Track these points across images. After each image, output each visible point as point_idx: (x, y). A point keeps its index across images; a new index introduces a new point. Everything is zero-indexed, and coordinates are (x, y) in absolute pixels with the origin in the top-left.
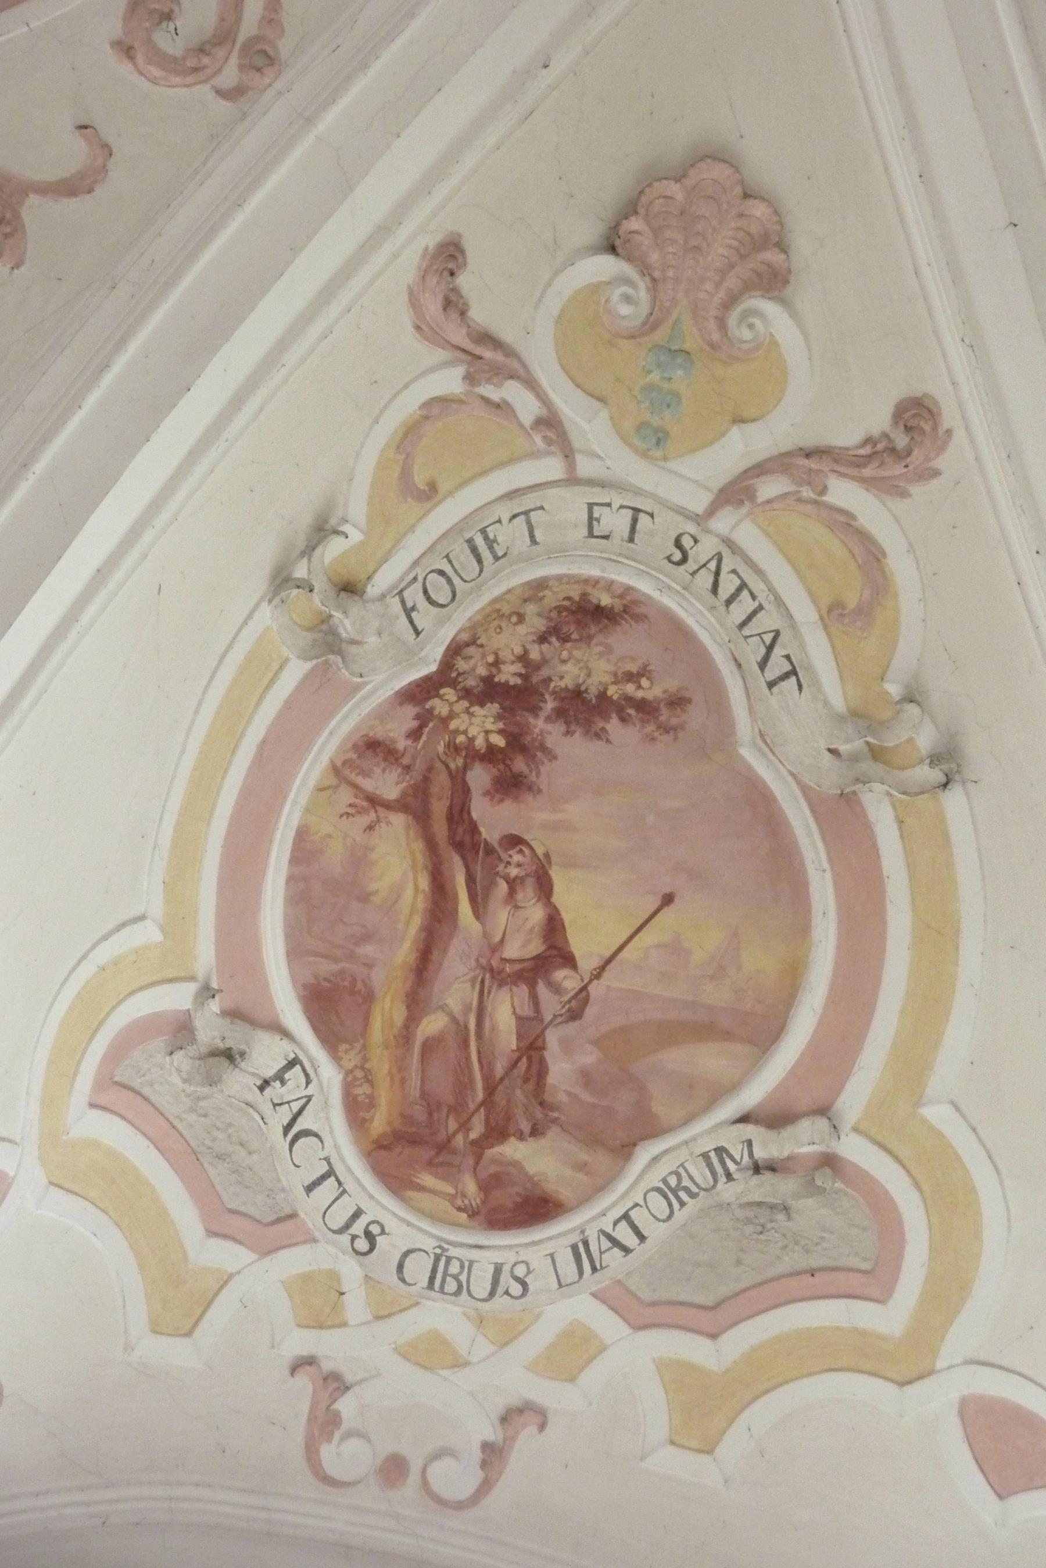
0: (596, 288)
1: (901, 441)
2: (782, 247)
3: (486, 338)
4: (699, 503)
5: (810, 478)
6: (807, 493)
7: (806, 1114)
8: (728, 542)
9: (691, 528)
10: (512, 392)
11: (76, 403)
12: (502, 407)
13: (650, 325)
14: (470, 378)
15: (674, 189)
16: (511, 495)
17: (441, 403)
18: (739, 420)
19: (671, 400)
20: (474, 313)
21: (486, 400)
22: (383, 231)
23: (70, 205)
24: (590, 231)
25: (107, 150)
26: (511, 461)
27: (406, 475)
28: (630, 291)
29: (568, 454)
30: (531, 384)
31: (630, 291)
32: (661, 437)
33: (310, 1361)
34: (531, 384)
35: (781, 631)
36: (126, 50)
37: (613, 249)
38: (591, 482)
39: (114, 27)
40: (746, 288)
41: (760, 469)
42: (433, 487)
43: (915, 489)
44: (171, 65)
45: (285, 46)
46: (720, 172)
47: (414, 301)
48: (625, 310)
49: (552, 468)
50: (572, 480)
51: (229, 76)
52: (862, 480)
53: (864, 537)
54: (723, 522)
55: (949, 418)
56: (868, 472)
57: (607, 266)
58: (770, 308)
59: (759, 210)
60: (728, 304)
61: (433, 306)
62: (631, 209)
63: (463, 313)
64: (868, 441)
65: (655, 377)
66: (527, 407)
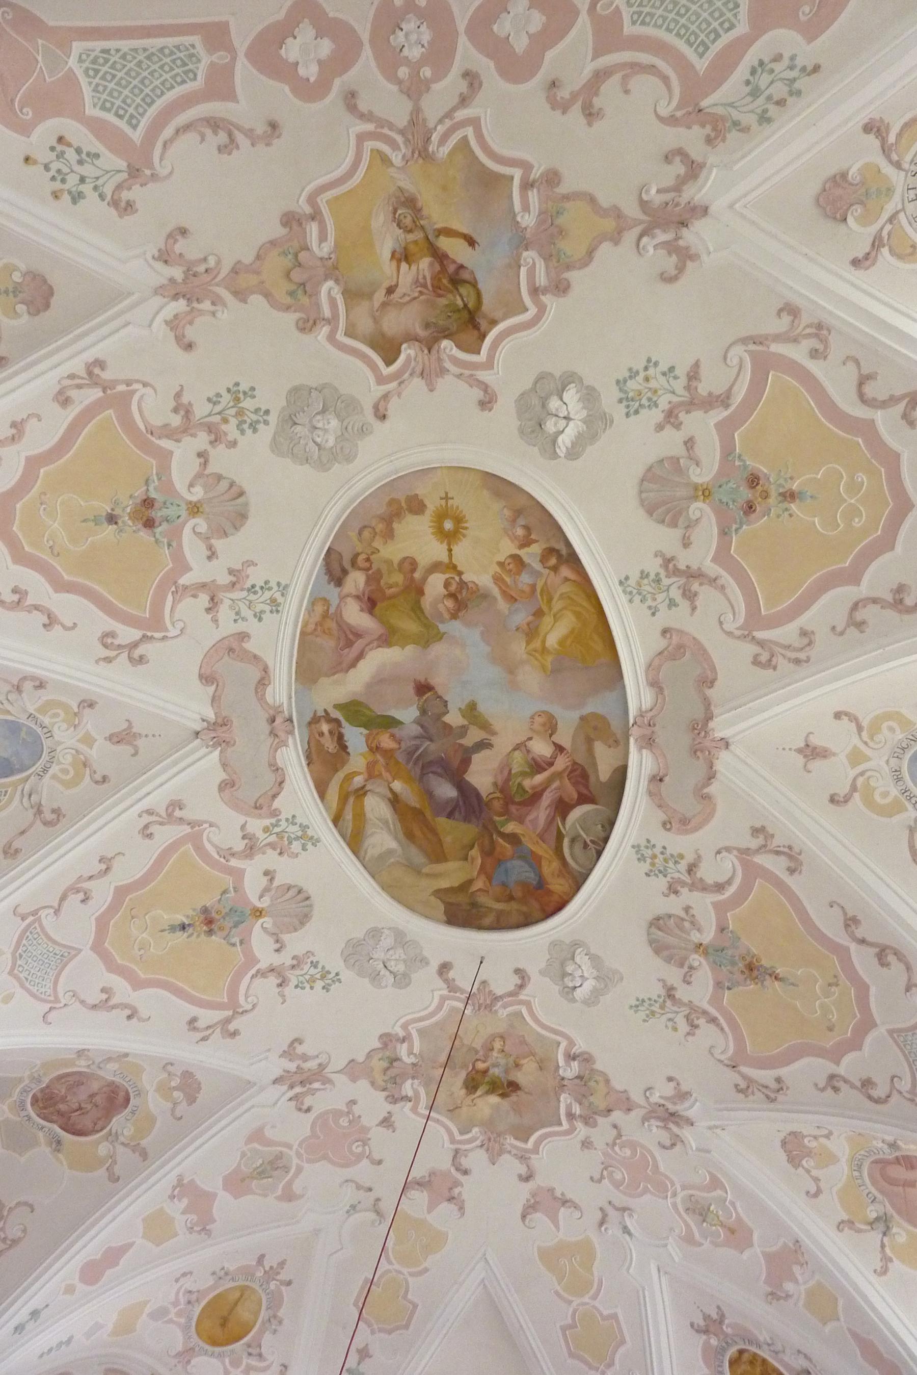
0: (856, 219)
1: (875, 129)
2: (835, 176)
3: (873, 245)
4: (903, 174)
5: (890, 149)
6: (894, 148)
8: (911, 163)
9: (909, 174)
10: (885, 233)
12: (889, 234)
13: (862, 203)
14: (884, 246)
15: (828, 209)
16: (910, 224)
17: (890, 251)
18: (879, 171)
19: (879, 191)
20: (867, 250)
21: (888, 239)
24: (842, 227)
25: (848, 357)
26: (901, 227)
28: (385, 148)
29: (897, 212)
30: (882, 229)
31: (385, 148)
32: (889, 189)
34: (882, 229)
35: (378, 1035)
36: (825, 358)
37: (845, 219)
38: (903, 204)
39: (821, 361)
40: (847, 181)
41: (891, 162)
42: (912, 246)
43: (886, 122)
45: (816, 321)
47: (867, 269)
48: (859, 211)
50: (903, 209)
51: (825, 332)
52: (887, 135)
53: (902, 130)
54: (906, 166)
55: (866, 120)
56: (884, 135)
57: (850, 220)
58: (850, 174)
59: (827, 186)
60: (853, 185)
61: (868, 263)
62: (835, 218)
64: (877, 137)
65: (874, 196)
66: (888, 227)
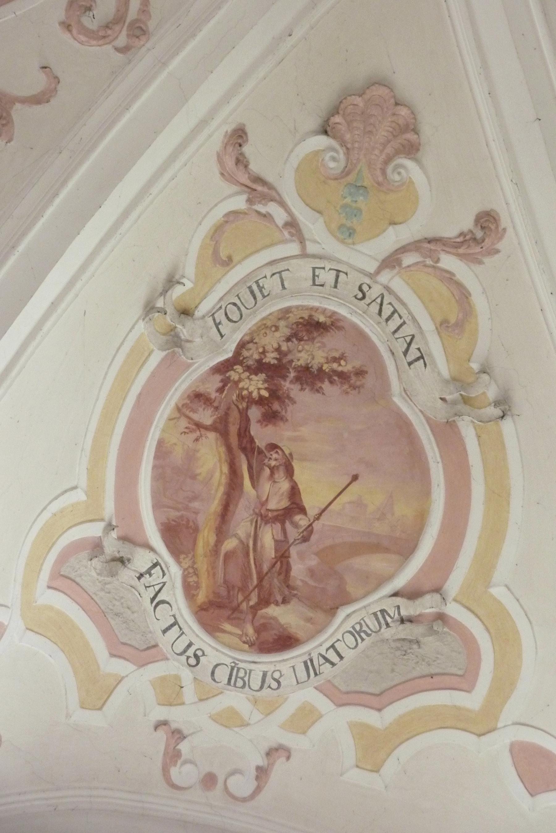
0: (317, 153)
1: (479, 234)
2: (416, 131)
3: (258, 180)
4: (372, 267)
5: (430, 254)
9: (367, 280)
10: (272, 208)
11: (40, 214)
12: (267, 216)
13: (346, 173)
14: (250, 201)
15: (358, 101)
16: (272, 263)
18: (393, 223)
19: (357, 212)
21: (258, 213)
24: (314, 123)
25: (57, 80)
26: (272, 245)
29: (302, 241)
30: (282, 204)
32: (351, 232)
34: (282, 204)
36: (67, 26)
37: (326, 132)
38: (314, 256)
39: (60, 14)
40: (397, 153)
41: (404, 249)
42: (230, 259)
43: (486, 260)
45: (151, 25)
46: (383, 91)
47: (220, 160)
48: (332, 165)
49: (293, 249)
50: (304, 255)
51: (122, 40)
52: (458, 255)
53: (459, 285)
54: (385, 277)
55: (505, 222)
56: (461, 251)
57: (322, 141)
58: (409, 164)
59: (403, 112)
60: (387, 162)
61: (230, 163)
64: (461, 234)
65: (348, 200)
66: (280, 216)
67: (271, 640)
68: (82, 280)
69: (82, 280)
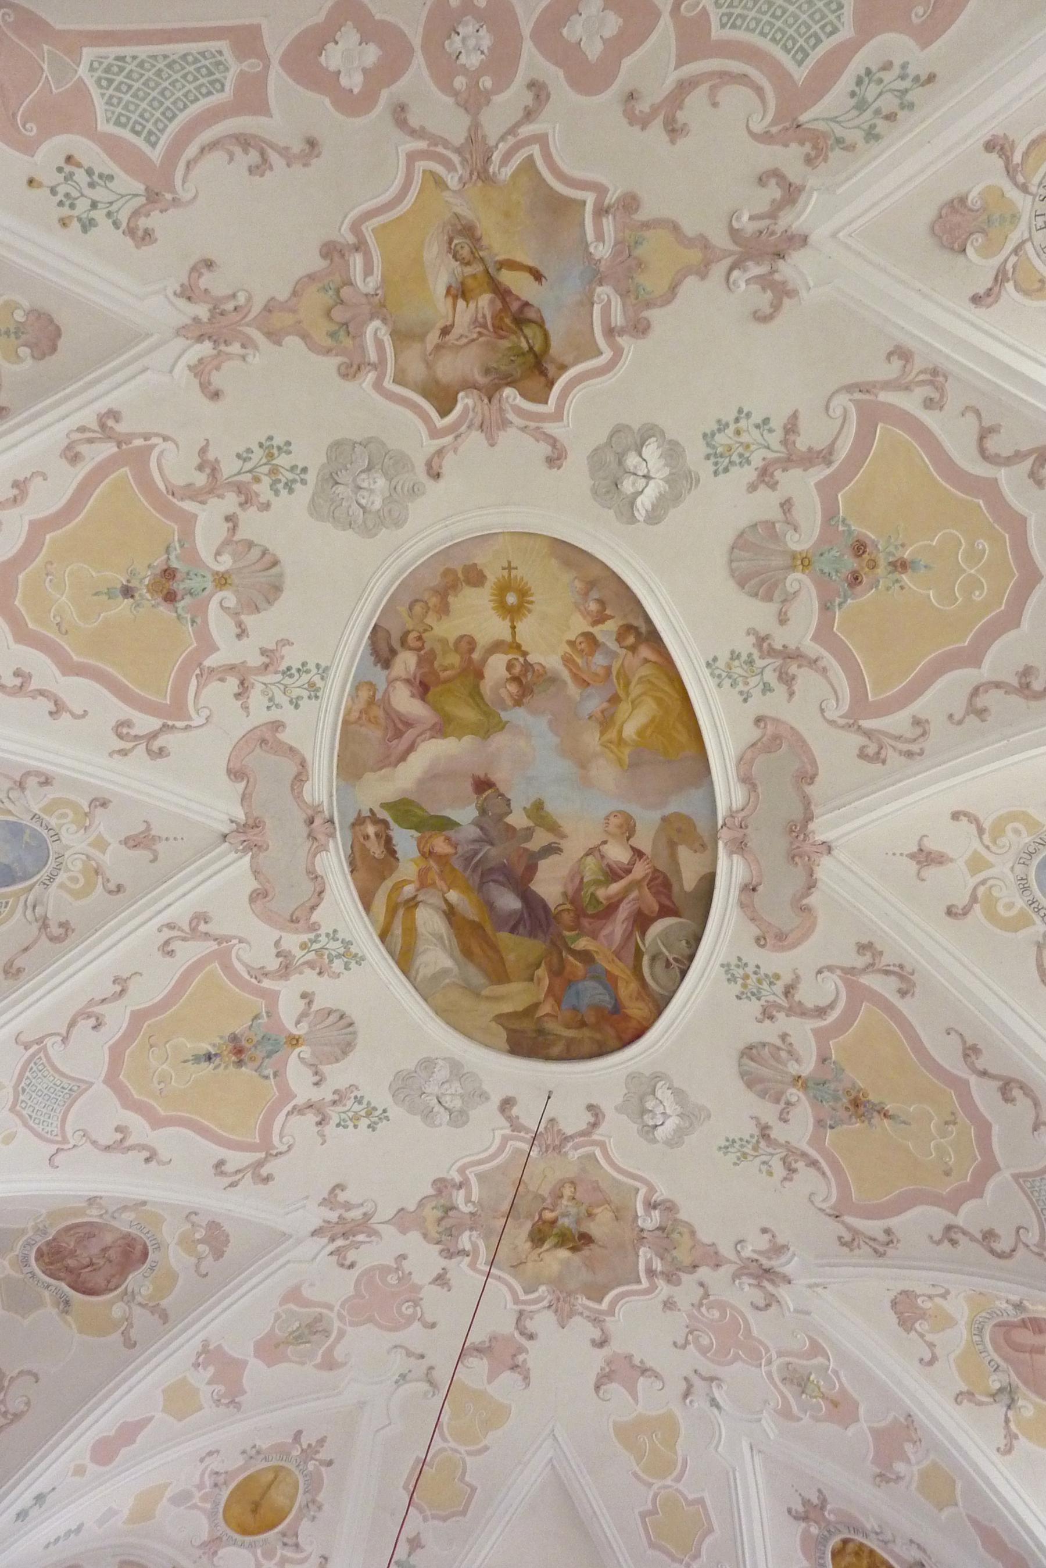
0: (976, 250)
1: (998, 148)
2: (952, 201)
3: (996, 279)
4: (1030, 198)
5: (1015, 170)
7: (964, 717)
8: (1039, 186)
9: (1037, 199)
10: (1009, 266)
11: (1032, 405)
12: (1014, 267)
13: (983, 231)
14: (1008, 280)
15: (944, 238)
16: (1038, 255)
17: (1016, 286)
18: (1003, 195)
19: (1002, 218)
21: (1013, 273)
22: (973, 324)
23: (983, 415)
24: (961, 258)
25: (967, 407)
26: (1028, 259)
27: (1040, 290)
29: (1023, 242)
30: (1006, 261)
32: (1014, 216)
33: (757, 1261)
34: (1006, 261)
36: (941, 408)
37: (964, 250)
38: (1030, 232)
39: (937, 412)
40: (966, 207)
41: (1016, 184)
42: (1040, 281)
43: (1011, 139)
44: (942, 396)
45: (931, 366)
46: (937, 227)
47: (989, 306)
48: (980, 240)
49: (1028, 246)
50: (1030, 239)
51: (941, 379)
52: (1012, 154)
53: (1028, 148)
54: (1033, 189)
55: (988, 137)
56: (1009, 154)
57: (970, 250)
58: (970, 198)
59: (944, 212)
60: (973, 211)
61: (990, 300)
63: (990, 290)
64: (1000, 157)
65: (997, 224)
66: (1013, 259)
67: (647, 1074)
68: (403, 1257)
69: (403, 1257)
